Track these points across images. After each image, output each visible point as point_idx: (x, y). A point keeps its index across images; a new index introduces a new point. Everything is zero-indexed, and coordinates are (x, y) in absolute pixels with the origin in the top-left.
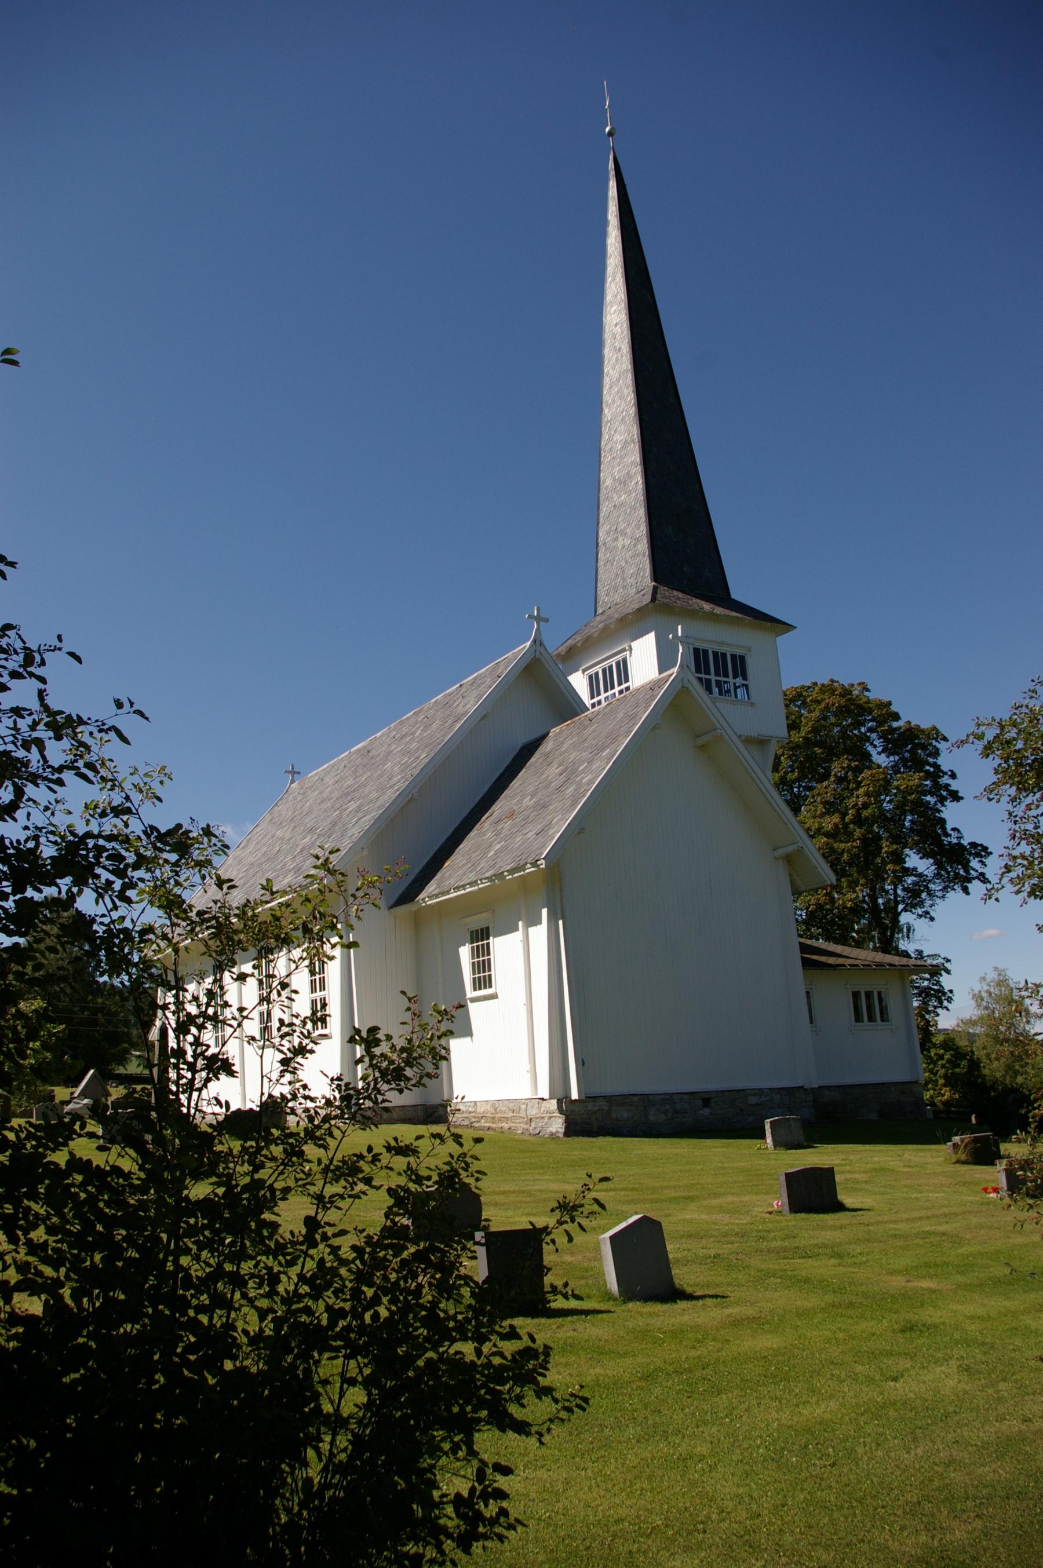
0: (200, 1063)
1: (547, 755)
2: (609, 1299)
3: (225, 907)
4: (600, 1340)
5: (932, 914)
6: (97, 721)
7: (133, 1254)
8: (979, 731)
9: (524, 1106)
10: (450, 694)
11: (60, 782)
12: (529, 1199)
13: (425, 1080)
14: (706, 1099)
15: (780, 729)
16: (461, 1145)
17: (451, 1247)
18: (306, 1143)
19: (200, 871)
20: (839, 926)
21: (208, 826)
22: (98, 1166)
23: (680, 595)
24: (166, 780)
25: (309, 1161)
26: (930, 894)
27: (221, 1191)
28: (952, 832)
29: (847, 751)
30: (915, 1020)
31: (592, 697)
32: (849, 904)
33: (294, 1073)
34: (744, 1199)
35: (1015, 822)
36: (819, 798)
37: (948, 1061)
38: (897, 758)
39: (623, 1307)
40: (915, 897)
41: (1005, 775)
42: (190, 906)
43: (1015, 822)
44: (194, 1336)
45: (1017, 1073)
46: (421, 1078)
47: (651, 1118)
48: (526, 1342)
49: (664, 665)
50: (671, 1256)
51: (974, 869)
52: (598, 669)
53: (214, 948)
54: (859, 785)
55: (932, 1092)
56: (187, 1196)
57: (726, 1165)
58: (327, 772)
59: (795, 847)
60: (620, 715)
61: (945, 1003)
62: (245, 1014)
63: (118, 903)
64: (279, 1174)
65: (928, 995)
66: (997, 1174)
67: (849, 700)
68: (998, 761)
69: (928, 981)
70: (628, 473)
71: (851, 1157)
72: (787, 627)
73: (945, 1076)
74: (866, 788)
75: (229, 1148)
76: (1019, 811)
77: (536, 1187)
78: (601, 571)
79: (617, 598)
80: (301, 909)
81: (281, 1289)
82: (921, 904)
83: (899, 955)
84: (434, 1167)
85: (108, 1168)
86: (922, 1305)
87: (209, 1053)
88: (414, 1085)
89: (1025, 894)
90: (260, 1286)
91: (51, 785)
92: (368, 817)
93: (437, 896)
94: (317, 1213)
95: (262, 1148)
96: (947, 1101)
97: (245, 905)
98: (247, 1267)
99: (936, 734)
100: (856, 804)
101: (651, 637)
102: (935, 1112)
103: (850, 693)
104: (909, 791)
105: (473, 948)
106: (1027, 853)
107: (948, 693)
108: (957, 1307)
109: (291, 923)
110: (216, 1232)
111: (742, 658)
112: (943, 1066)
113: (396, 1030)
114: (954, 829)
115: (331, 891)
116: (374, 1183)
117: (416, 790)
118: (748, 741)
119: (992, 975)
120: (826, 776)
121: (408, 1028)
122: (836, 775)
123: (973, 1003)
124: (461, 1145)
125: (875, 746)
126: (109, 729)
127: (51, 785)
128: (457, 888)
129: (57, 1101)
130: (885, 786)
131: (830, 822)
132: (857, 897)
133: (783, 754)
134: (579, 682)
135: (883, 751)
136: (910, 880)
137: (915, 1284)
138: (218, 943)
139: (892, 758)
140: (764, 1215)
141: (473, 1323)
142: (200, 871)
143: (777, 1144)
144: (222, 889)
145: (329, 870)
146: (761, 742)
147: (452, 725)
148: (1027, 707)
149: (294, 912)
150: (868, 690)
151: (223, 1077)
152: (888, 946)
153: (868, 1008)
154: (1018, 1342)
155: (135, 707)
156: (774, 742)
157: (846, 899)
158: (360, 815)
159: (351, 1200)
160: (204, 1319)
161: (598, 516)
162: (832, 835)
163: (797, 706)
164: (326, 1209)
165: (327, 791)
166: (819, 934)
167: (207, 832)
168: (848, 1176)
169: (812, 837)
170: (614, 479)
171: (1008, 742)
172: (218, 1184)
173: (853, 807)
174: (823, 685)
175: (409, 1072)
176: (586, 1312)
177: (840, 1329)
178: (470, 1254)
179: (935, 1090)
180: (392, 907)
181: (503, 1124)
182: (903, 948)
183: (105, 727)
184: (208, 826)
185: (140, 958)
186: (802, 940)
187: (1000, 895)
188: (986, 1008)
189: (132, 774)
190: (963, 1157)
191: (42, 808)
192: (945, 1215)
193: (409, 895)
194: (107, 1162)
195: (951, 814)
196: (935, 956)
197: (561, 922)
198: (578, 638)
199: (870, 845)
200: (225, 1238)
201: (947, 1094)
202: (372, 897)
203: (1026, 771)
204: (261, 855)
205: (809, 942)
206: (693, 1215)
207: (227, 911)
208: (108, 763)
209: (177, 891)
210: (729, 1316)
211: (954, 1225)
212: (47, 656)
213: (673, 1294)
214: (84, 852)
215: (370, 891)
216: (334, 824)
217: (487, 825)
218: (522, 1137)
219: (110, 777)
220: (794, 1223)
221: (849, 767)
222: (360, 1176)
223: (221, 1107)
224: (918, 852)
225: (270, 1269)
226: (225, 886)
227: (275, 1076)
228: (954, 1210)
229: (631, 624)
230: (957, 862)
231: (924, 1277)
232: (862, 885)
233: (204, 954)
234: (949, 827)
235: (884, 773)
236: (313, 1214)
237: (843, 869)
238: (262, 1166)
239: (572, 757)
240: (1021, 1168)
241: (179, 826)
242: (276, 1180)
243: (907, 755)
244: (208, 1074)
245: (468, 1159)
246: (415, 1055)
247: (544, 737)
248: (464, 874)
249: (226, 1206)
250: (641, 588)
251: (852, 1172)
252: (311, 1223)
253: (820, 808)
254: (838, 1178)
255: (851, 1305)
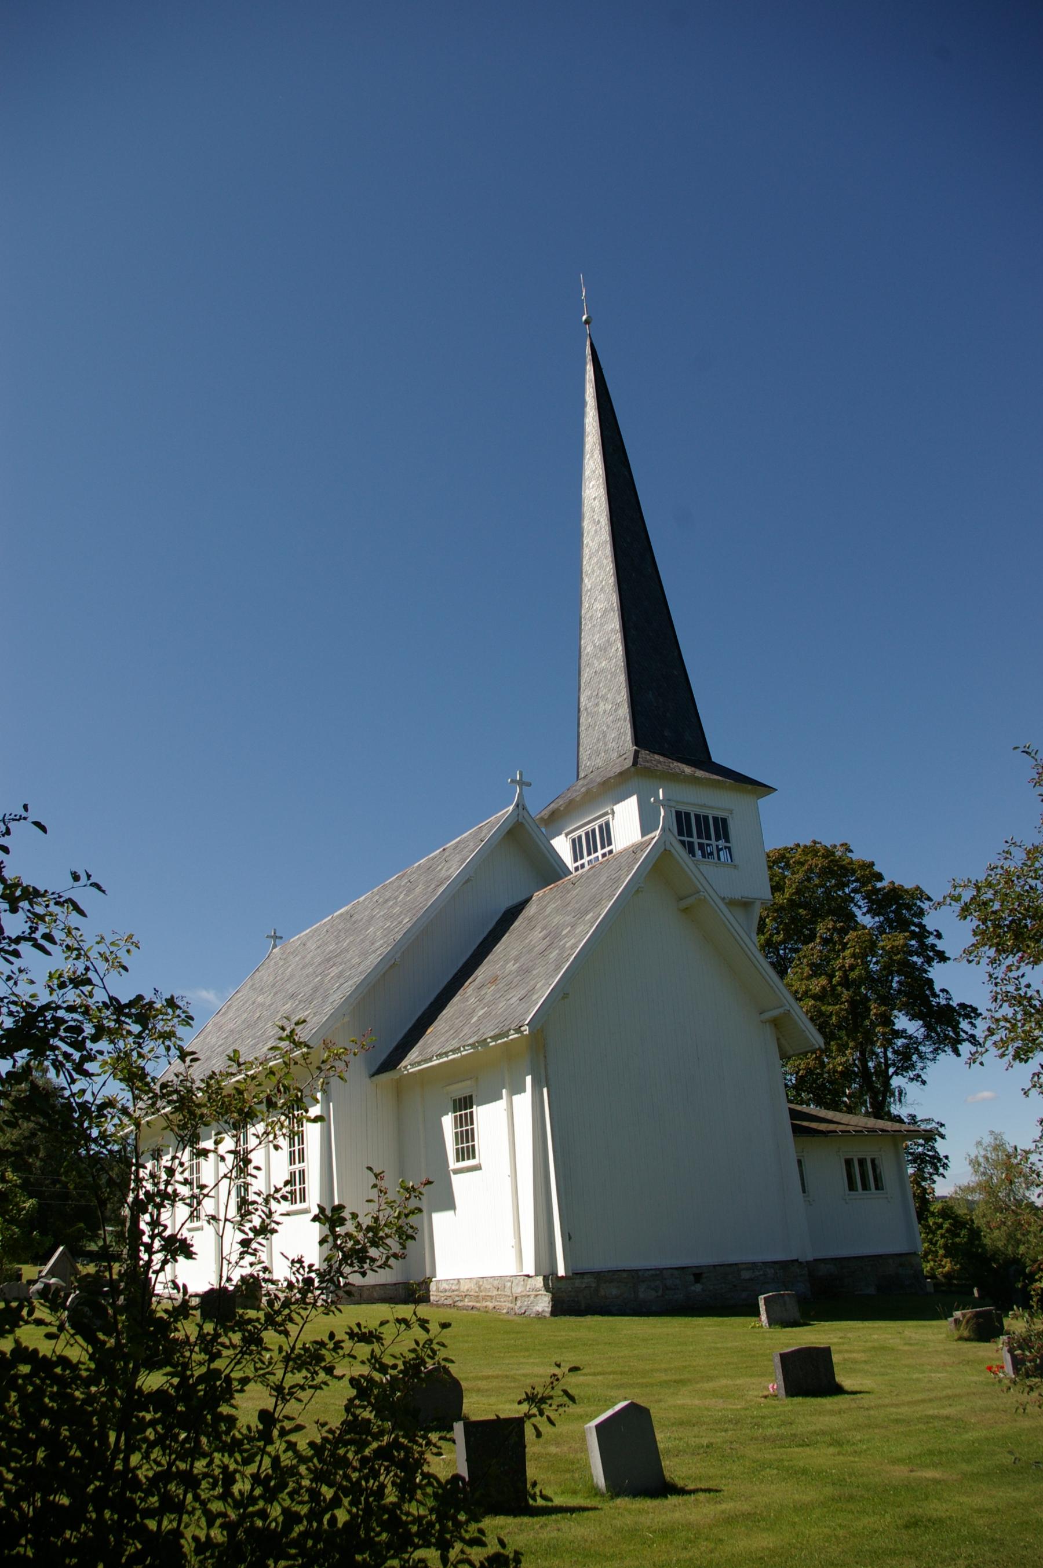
0: (157, 1244)
1: (530, 919)
2: (596, 1494)
3: (187, 1080)
4: (586, 1541)
5: (924, 1077)
6: (53, 893)
7: (75, 1453)
8: (956, 893)
9: (509, 1284)
10: (433, 858)
11: (16, 954)
12: (513, 1384)
13: (392, 1261)
14: (698, 1274)
15: (765, 892)
16: (427, 1331)
17: (416, 1442)
18: (266, 1329)
19: (163, 1043)
20: (829, 1090)
21: (172, 997)
22: (44, 1356)
23: (662, 759)
24: (133, 948)
25: (267, 1350)
26: (922, 1057)
27: (176, 1381)
28: (941, 994)
29: (831, 912)
30: (911, 1188)
31: (576, 861)
32: (840, 1068)
33: (255, 1255)
34: (738, 1382)
35: (996, 984)
36: (805, 960)
37: (948, 1230)
38: (882, 918)
39: (611, 1504)
40: (906, 1061)
41: (984, 937)
42: (153, 1079)
43: (996, 984)
44: (140, 1543)
45: (1019, 1242)
46: (388, 1258)
47: (641, 1296)
48: (493, 1548)
49: (645, 830)
50: (661, 1446)
51: (964, 1032)
52: (581, 832)
53: (176, 1122)
54: (844, 949)
55: (932, 1263)
56: (140, 1388)
57: (719, 1345)
58: (309, 937)
59: (781, 1010)
60: (603, 879)
61: (941, 1170)
62: (205, 1191)
63: (76, 1076)
64: (236, 1364)
65: (923, 1161)
66: (998, 1351)
67: (832, 861)
68: (976, 922)
69: (922, 1148)
70: (608, 641)
71: (849, 1335)
72: (767, 789)
73: (945, 1246)
74: (852, 950)
75: (186, 1335)
76: (1000, 972)
77: (522, 1372)
78: (582, 736)
79: (599, 762)
80: (265, 1082)
81: (236, 1489)
82: (912, 1067)
83: (892, 1120)
84: (399, 1356)
85: (54, 1359)
86: (927, 1498)
87: (167, 1234)
88: (380, 1267)
89: (1010, 1057)
90: (214, 1486)
91: (7, 956)
92: (350, 983)
93: (419, 1063)
94: (276, 1405)
95: (220, 1336)
96: (948, 1273)
97: (211, 1078)
98: (200, 1465)
99: (919, 894)
100: (843, 966)
101: (633, 802)
102: (936, 1285)
103: (833, 854)
104: (895, 950)
105: (456, 1117)
106: (1010, 1016)
107: (934, 852)
108: (963, 1499)
109: (254, 1097)
110: (168, 1428)
111: (724, 821)
112: (942, 1236)
113: (361, 1207)
114: (943, 990)
115: (296, 1063)
116: (336, 1372)
117: (399, 955)
118: (732, 903)
119: (988, 1140)
120: (811, 938)
121: (374, 1206)
122: (821, 937)
123: (970, 1169)
124: (427, 1331)
125: (860, 907)
126: (66, 901)
127: (7, 956)
128: (440, 1056)
129: (24, 1281)
130: (871, 947)
131: (817, 985)
132: (848, 1060)
133: (768, 916)
134: (562, 845)
135: (868, 912)
136: (900, 1042)
137: (918, 1474)
138: (181, 1117)
139: (877, 919)
140: (759, 1399)
141: (437, 1527)
142: (163, 1043)
143: (771, 1322)
144: (184, 1062)
145: (294, 1042)
146: (745, 905)
147: (435, 890)
148: (1002, 868)
149: (260, 1085)
150: (851, 851)
151: (181, 1259)
152: (880, 1110)
153: (862, 1176)
154: (1029, 1538)
155: (93, 880)
156: (758, 903)
157: (837, 1062)
158: (342, 981)
159: (313, 1391)
160: (152, 1525)
161: (580, 681)
162: (819, 997)
163: (780, 868)
164: (285, 1401)
165: (309, 956)
166: (810, 1099)
167: (171, 1003)
168: (847, 1356)
169: (800, 1000)
170: (595, 646)
171: (985, 904)
172: (172, 1375)
173: (840, 969)
174: (805, 847)
175: (373, 1252)
176: (572, 1510)
177: (840, 1525)
178: (435, 1450)
179: (935, 1261)
180: (373, 1075)
181: (488, 1303)
182: (896, 1113)
183: (62, 900)
184: (172, 997)
185: (100, 1132)
186: (792, 1106)
187: (984, 1058)
188: (984, 1174)
189: (98, 943)
190: (966, 1334)
191: (4, 978)
192: (949, 1397)
193: (391, 1062)
194: (54, 1351)
195: (939, 974)
196: (929, 1121)
197: (545, 1090)
198: (561, 802)
199: (858, 1008)
200: (178, 1434)
201: (948, 1265)
202: (338, 1070)
203: (1005, 932)
204: (226, 1028)
205: (799, 1108)
206: (685, 1400)
207: (189, 1084)
208: (74, 932)
209: (141, 1062)
210: (723, 1512)
211: (959, 1408)
212: (12, 825)
213: (663, 1488)
214: (42, 1024)
215: (337, 1063)
216: (315, 990)
217: (470, 991)
218: (506, 1317)
219: (76, 946)
220: (790, 1408)
221: (834, 929)
222: (323, 1364)
223: (179, 1291)
224: (907, 1014)
225: (225, 1468)
226: (188, 1059)
227: (234, 1258)
228: (957, 1391)
229: (613, 788)
230: (946, 1023)
231: (927, 1466)
232: (852, 1048)
233: (165, 1128)
234: (937, 988)
235: (870, 934)
236: (271, 1408)
237: (832, 1033)
238: (219, 1355)
239: (556, 921)
240: (1020, 1347)
241: (140, 997)
242: (232, 1370)
243: (892, 915)
244: (166, 1256)
245: (436, 1347)
246: (381, 1234)
247: (527, 901)
248: (447, 1041)
249: (179, 1399)
250: (622, 752)
251: (851, 1352)
252: (266, 1417)
253: (807, 970)
254: (836, 1358)
255: (851, 1498)
